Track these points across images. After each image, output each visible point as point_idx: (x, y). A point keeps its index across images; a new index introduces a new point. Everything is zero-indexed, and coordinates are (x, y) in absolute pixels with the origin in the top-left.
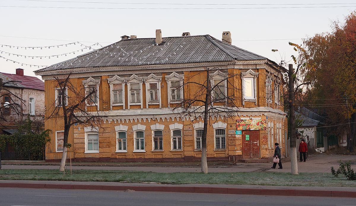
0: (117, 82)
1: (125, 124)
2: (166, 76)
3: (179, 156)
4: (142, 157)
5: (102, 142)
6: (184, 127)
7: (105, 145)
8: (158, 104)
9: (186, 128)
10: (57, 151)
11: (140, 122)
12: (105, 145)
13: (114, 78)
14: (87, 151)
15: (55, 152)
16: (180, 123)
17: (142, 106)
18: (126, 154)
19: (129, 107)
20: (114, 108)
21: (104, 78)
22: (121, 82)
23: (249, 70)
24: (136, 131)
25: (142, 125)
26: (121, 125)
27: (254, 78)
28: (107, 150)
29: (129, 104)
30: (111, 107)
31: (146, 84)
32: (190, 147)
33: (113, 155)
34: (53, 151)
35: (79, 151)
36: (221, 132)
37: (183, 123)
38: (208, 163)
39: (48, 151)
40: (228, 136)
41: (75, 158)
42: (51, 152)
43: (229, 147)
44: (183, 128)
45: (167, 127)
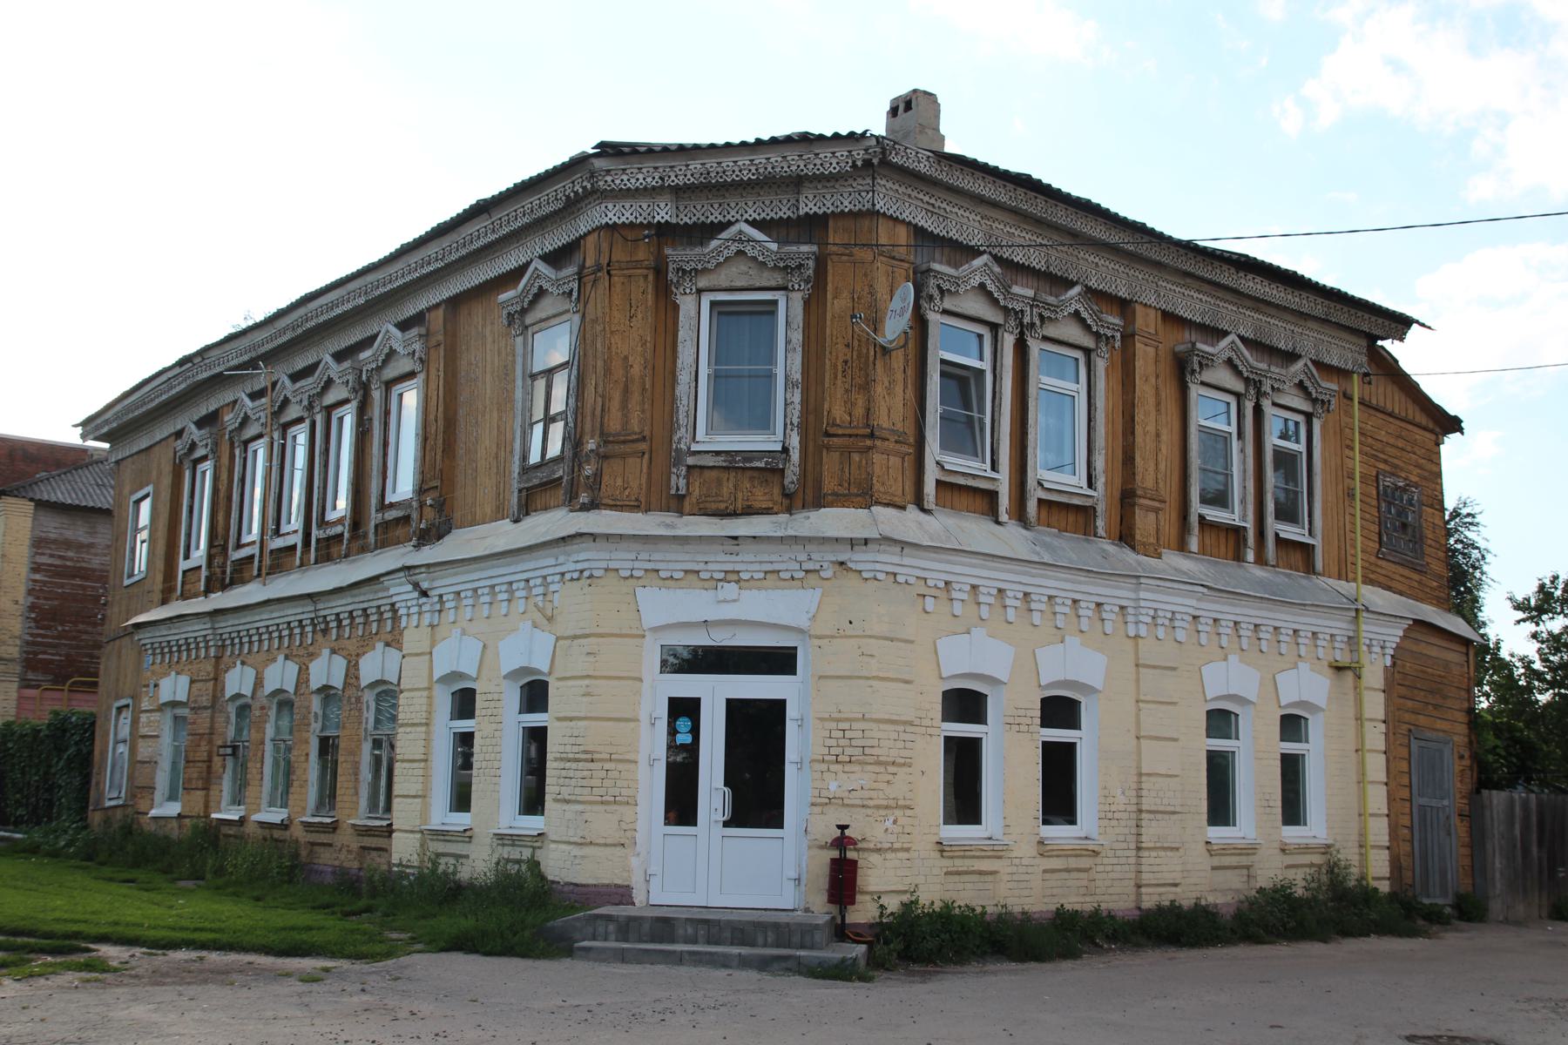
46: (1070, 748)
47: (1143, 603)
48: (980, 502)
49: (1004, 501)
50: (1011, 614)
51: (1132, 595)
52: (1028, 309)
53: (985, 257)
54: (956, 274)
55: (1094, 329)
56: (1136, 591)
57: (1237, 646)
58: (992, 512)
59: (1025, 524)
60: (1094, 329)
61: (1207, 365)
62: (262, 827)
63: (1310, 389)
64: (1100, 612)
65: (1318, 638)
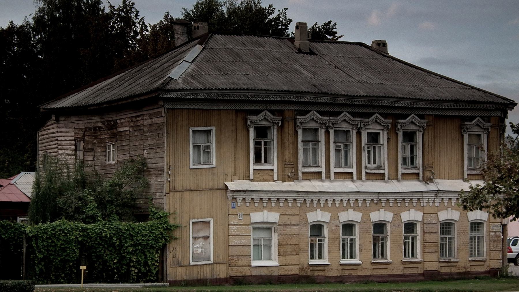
0: (313, 125)
1: (387, 207)
2: (298, 117)
3: (414, 271)
4: (354, 273)
5: (284, 243)
6: (425, 216)
7: (289, 249)
8: (382, 171)
9: (428, 219)
10: (192, 263)
11: (352, 205)
12: (289, 249)
13: (309, 116)
14: (254, 264)
15: (189, 265)
16: (420, 210)
17: (356, 176)
18: (326, 268)
19: (332, 175)
20: (405, 177)
21: (287, 115)
22: (318, 125)
23: (375, 115)
24: (374, 223)
25: (356, 212)
26: (319, 210)
27: (352, 128)
28: (293, 259)
29: (333, 170)
30: (300, 174)
31: (399, 135)
32: (434, 255)
33: (302, 269)
34: (182, 263)
35: (240, 263)
36: (446, 228)
37: (422, 209)
38: (78, 283)
39: (173, 262)
40: (490, 235)
41: (231, 277)
42: (178, 264)
43: (492, 254)
44: (423, 219)
45: (397, 216)
46: (414, 242)
47: (424, 198)
48: (415, 177)
49: (324, 175)
50: (248, 204)
51: (421, 196)
52: (328, 122)
53: (478, 118)
54: (484, 124)
55: (483, 127)
56: (423, 194)
57: (262, 206)
58: (418, 179)
59: (398, 180)
60: (483, 127)
61: (469, 128)
62: (341, 266)
63: (380, 122)
64: (319, 202)
65: (313, 201)
